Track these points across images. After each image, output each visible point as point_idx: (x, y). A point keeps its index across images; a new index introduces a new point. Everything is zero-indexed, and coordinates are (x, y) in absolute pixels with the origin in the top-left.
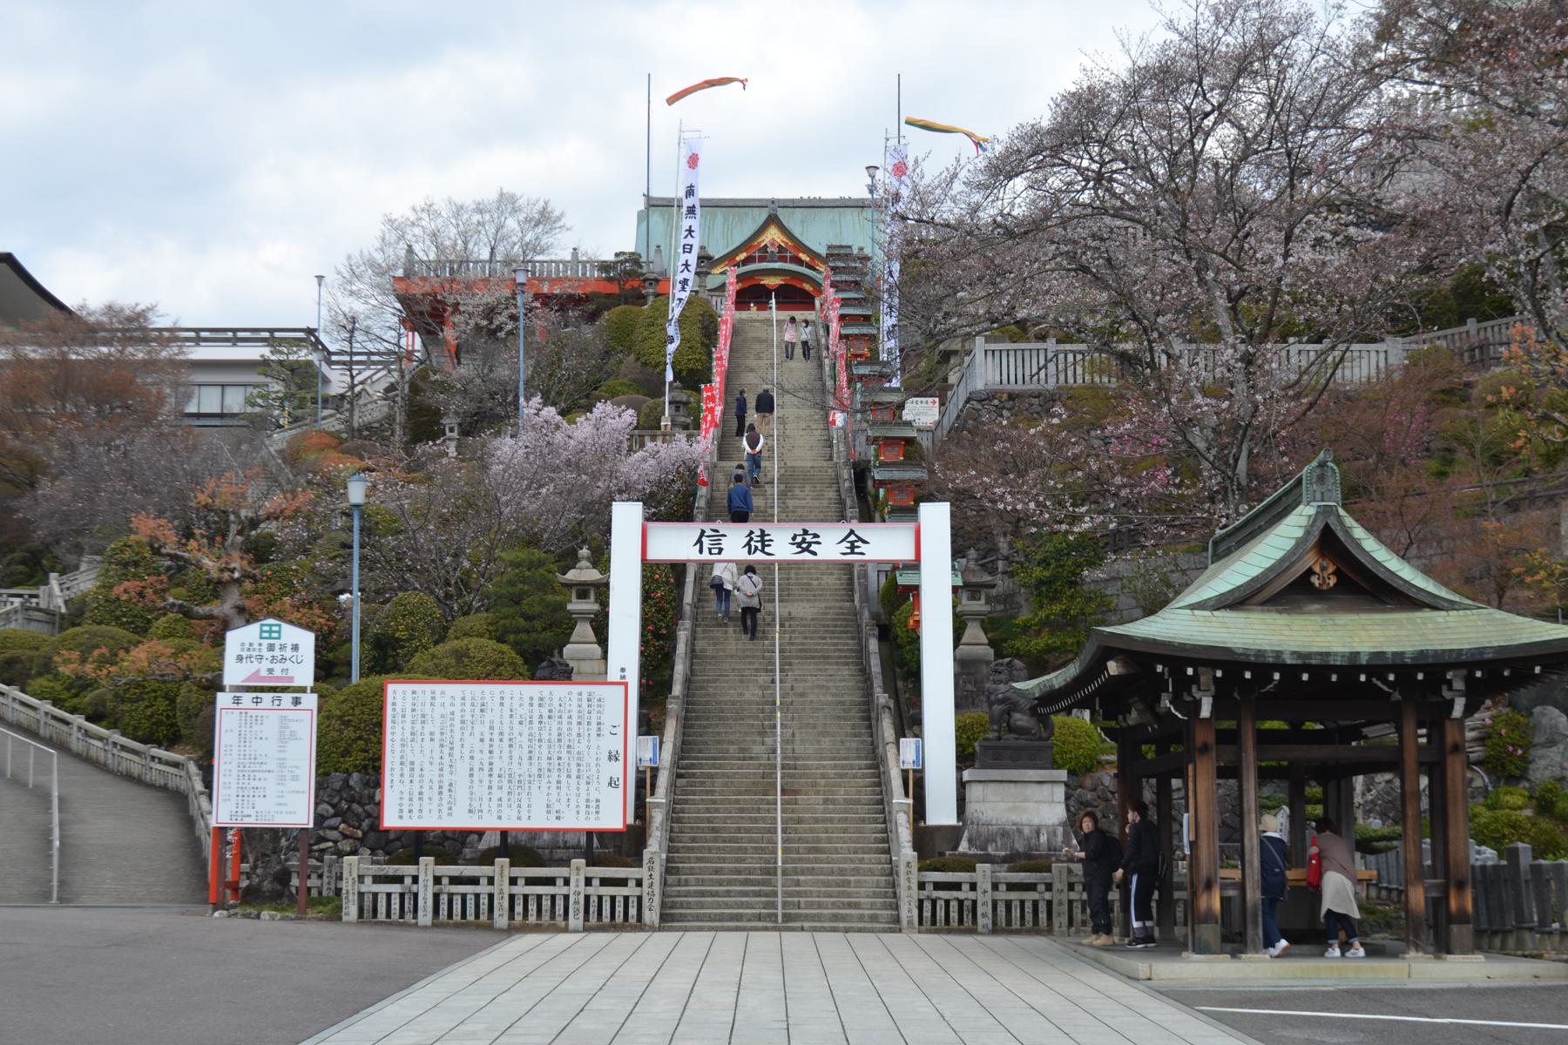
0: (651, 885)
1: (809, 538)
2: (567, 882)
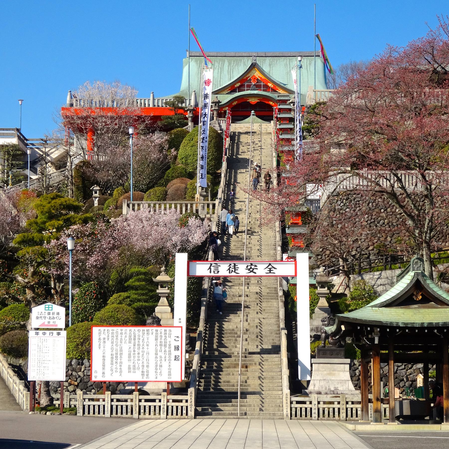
0: (191, 402)
1: (253, 267)
2: (160, 401)
